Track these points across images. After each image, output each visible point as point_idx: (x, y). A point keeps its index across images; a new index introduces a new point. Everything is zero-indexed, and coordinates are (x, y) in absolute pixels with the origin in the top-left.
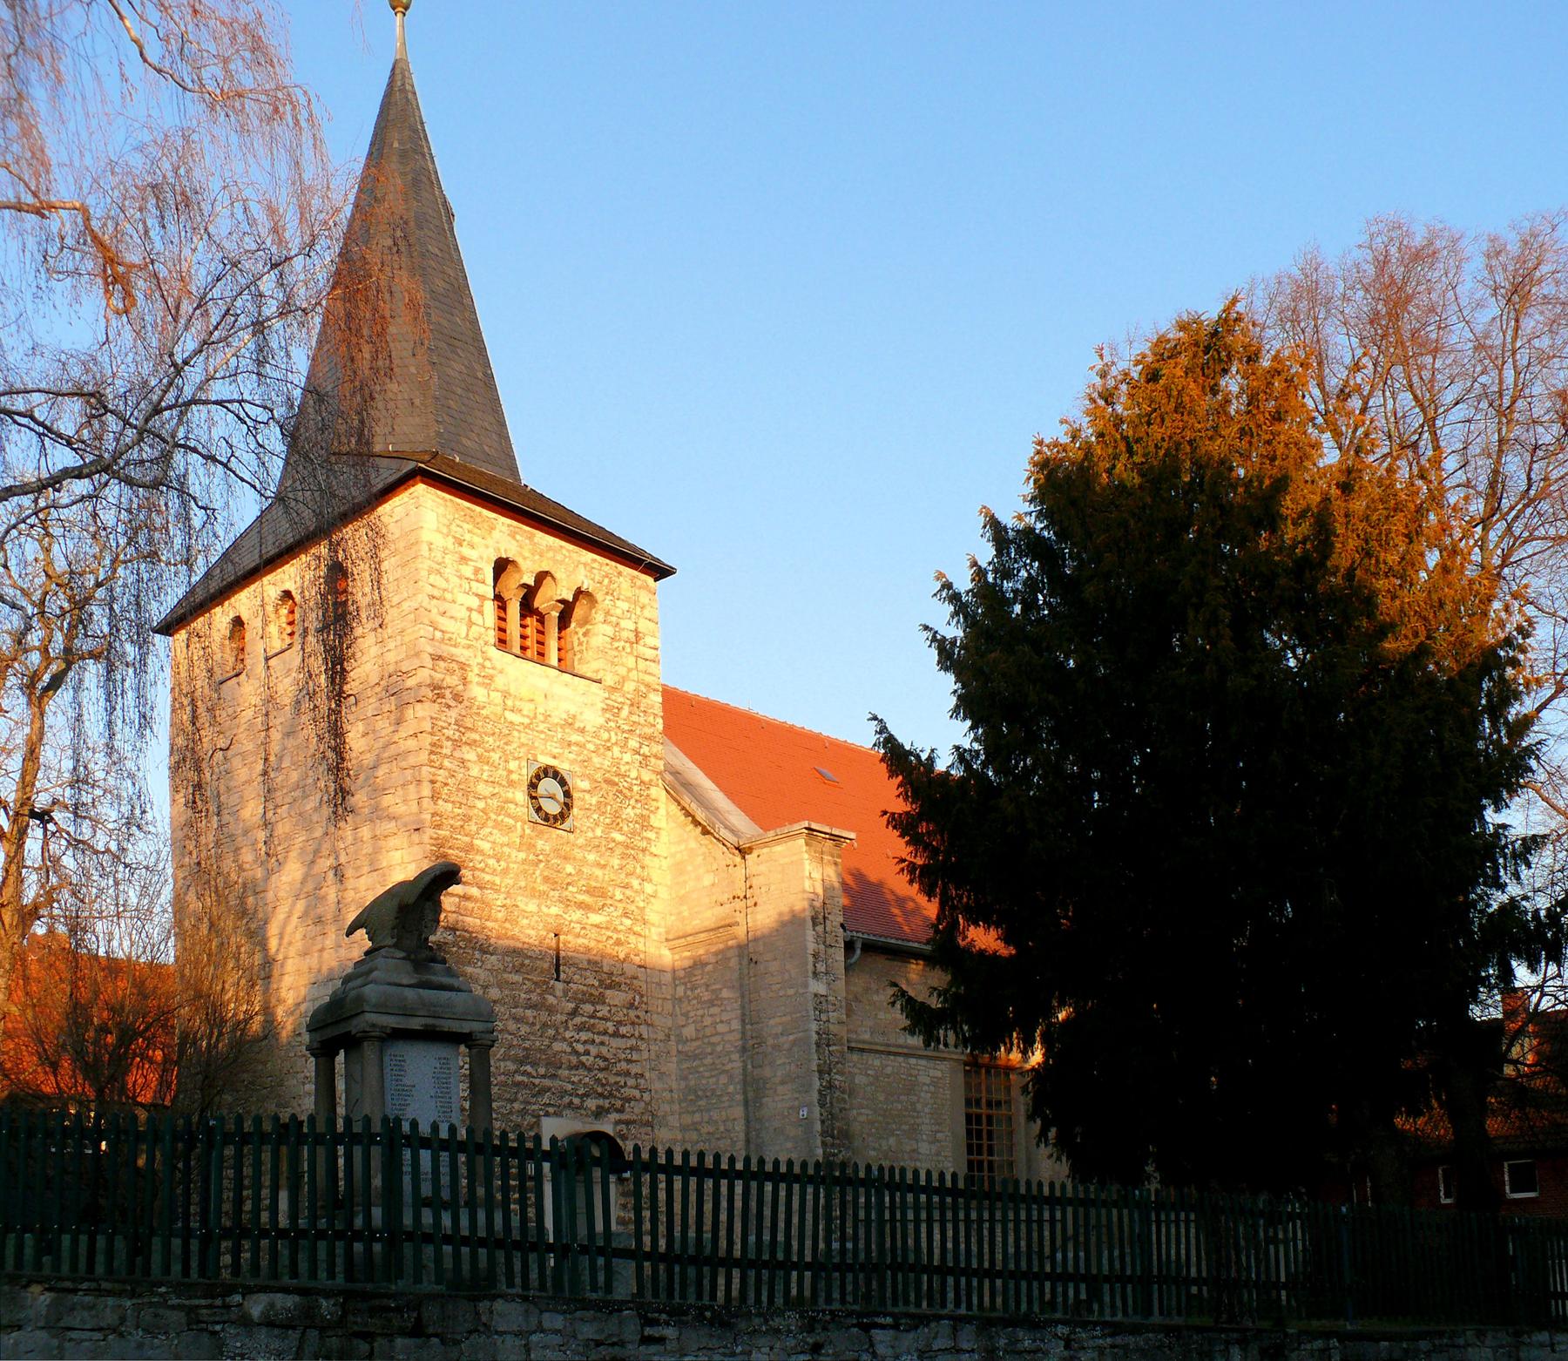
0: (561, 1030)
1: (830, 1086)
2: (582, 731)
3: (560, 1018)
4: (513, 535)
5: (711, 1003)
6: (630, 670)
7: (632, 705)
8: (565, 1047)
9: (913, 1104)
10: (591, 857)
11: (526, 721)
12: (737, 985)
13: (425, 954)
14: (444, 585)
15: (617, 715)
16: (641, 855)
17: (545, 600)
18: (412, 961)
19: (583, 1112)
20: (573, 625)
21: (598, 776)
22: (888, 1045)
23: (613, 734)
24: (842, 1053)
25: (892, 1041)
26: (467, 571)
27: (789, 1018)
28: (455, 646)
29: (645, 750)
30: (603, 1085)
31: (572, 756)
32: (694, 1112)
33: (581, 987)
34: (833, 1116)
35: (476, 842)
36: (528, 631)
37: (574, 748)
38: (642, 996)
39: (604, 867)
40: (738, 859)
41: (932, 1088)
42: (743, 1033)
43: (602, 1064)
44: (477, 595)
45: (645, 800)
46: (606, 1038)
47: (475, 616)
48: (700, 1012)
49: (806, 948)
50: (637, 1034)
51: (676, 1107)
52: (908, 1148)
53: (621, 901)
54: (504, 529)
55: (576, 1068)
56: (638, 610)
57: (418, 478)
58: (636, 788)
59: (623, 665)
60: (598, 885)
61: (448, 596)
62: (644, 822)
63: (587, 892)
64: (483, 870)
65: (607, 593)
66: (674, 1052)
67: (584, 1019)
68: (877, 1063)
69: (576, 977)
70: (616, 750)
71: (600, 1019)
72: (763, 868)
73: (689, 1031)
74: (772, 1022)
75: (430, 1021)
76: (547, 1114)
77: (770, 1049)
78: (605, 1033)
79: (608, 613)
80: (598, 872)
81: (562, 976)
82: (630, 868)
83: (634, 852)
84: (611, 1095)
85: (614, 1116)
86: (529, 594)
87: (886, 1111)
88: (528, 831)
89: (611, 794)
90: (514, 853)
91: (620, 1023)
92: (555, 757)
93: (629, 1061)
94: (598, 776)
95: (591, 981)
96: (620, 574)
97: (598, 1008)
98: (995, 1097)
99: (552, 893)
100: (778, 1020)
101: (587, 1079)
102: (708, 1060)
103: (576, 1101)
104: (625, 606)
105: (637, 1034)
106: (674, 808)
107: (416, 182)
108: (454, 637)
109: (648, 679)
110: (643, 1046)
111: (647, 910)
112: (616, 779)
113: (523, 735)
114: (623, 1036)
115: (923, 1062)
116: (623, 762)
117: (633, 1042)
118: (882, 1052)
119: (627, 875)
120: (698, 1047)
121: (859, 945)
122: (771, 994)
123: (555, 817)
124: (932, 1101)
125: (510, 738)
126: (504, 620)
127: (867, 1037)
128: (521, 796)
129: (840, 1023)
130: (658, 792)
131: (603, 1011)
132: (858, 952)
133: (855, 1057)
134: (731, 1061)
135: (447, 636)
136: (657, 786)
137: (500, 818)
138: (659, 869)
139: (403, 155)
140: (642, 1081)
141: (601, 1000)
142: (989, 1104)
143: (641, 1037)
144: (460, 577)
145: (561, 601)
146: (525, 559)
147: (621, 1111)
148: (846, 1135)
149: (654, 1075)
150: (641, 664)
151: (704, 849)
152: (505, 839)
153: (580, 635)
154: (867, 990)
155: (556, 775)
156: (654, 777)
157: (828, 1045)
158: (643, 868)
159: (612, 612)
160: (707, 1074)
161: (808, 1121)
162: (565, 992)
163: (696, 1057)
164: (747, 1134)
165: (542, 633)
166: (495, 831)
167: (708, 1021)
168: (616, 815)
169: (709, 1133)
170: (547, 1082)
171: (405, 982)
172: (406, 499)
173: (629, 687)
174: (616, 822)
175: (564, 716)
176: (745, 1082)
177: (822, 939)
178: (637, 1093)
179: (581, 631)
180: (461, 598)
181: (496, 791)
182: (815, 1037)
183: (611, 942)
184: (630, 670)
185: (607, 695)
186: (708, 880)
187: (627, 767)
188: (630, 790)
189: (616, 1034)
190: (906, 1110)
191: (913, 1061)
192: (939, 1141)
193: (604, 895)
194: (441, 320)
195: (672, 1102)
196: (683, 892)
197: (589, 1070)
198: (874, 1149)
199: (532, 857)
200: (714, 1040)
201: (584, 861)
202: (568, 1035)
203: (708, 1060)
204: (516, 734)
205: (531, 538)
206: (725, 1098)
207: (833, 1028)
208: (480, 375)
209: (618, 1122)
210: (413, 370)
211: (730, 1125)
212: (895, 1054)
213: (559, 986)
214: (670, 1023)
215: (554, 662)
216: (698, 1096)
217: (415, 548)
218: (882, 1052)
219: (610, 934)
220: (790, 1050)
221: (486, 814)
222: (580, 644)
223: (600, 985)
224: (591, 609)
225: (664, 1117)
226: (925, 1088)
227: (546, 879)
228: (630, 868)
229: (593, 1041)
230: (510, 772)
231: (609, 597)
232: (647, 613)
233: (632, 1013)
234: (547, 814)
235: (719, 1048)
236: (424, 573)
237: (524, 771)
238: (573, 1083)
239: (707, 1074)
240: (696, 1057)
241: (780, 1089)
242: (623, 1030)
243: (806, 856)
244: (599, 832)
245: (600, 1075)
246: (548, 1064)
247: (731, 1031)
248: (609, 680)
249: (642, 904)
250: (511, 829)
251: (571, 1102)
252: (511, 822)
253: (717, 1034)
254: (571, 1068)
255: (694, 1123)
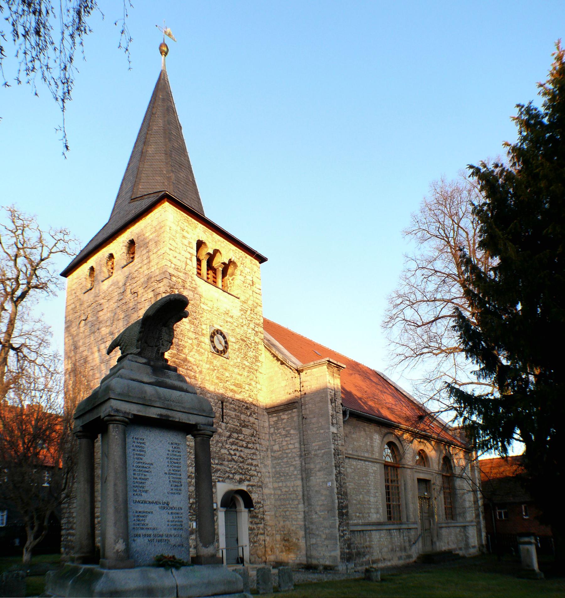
0: (224, 444)
1: (340, 473)
2: (232, 317)
3: (224, 439)
4: (204, 232)
5: (286, 436)
6: (250, 296)
7: (251, 310)
8: (226, 451)
9: (368, 481)
10: (236, 370)
11: (210, 309)
12: (297, 428)
13: (160, 363)
14: (176, 245)
15: (245, 313)
16: (255, 372)
17: (217, 262)
18: (152, 366)
19: (234, 480)
20: (228, 276)
21: (239, 337)
22: (358, 456)
23: (244, 320)
24: (343, 458)
25: (360, 454)
26: (186, 242)
27: (321, 443)
28: (180, 272)
29: (256, 329)
30: (242, 469)
31: (228, 327)
32: (279, 482)
33: (232, 426)
34: (341, 486)
35: (188, 358)
36: (209, 276)
37: (228, 324)
38: (257, 432)
39: (241, 375)
40: (297, 375)
41: (374, 475)
42: (300, 449)
43: (242, 460)
44: (189, 253)
45: (256, 350)
46: (243, 449)
47: (189, 262)
48: (281, 440)
49: (328, 412)
50: (255, 448)
51: (271, 480)
52: (366, 500)
53: (248, 390)
54: (201, 229)
55: (231, 461)
56: (253, 273)
57: (166, 199)
58: (253, 344)
59: (247, 293)
60: (239, 383)
61: (177, 250)
62: (256, 359)
63: (234, 385)
64: (191, 370)
65: (241, 264)
66: (270, 456)
67: (234, 440)
68: (355, 463)
69: (230, 421)
70: (245, 327)
71: (241, 440)
72: (308, 378)
73: (276, 447)
74: (313, 444)
75: (164, 412)
76: (219, 481)
77: (313, 456)
78: (242, 446)
79: (241, 271)
80: (239, 377)
81: (225, 420)
82: (251, 377)
83: (252, 370)
84: (245, 474)
85: (246, 483)
86: (211, 258)
87: (358, 483)
88: (210, 356)
89: (243, 345)
90: (204, 365)
91: (248, 443)
92: (221, 326)
93: (252, 459)
94: (239, 337)
95: (236, 423)
96: (246, 257)
97: (240, 435)
98: (393, 478)
99: (220, 384)
100: (316, 443)
101: (235, 466)
102: (285, 460)
103: (231, 476)
104: (248, 270)
105: (255, 448)
106: (268, 354)
107: (168, 110)
108: (180, 268)
109: (257, 301)
110: (258, 453)
111: (258, 395)
112: (245, 339)
113: (208, 315)
114: (250, 448)
115: (370, 464)
116: (248, 333)
117: (253, 451)
118: (356, 459)
119: (251, 380)
120: (280, 454)
121: (348, 413)
122: (313, 432)
123: (221, 351)
124: (374, 480)
125: (202, 315)
126: (200, 270)
127: (351, 452)
128: (207, 340)
129: (342, 445)
130: (261, 347)
131: (241, 437)
132: (348, 416)
133: (347, 460)
134: (295, 461)
135: (177, 267)
136: (261, 344)
137: (198, 349)
138: (262, 378)
139: (163, 100)
140: (257, 468)
141: (240, 432)
142: (392, 481)
143: (256, 449)
144: (183, 244)
145: (224, 263)
146: (209, 242)
147: (249, 481)
148: (346, 494)
149: (262, 465)
150: (255, 295)
151: (281, 371)
152: (201, 358)
153: (230, 280)
154: (350, 432)
155: (221, 334)
156: (260, 340)
157: (338, 455)
158: (256, 377)
159: (243, 271)
160: (284, 466)
161: (331, 488)
162: (226, 428)
163: (279, 458)
164: (303, 492)
165: (215, 278)
166: (196, 354)
167: (284, 443)
168: (246, 355)
169: (286, 491)
170: (219, 467)
171: (146, 379)
172: (160, 209)
173: (250, 303)
174: (245, 357)
175: (225, 310)
176: (302, 471)
177: (334, 409)
178: (255, 473)
179: (231, 278)
180: (183, 253)
181: (197, 337)
182: (333, 451)
183: (244, 407)
184: (250, 296)
185: (241, 304)
186: (283, 383)
187: (250, 335)
188: (251, 344)
189: (247, 447)
190: (365, 483)
191: (367, 463)
192: (377, 497)
193: (241, 387)
194: (176, 157)
195: (269, 477)
196: (272, 389)
197: (236, 462)
198: (355, 500)
199: (212, 367)
200: (287, 451)
201: (233, 371)
202: (227, 446)
203: (285, 460)
204: (205, 313)
205: (212, 235)
206: (293, 477)
207: (340, 448)
208: (191, 180)
209: (248, 486)
210: (165, 172)
211: (295, 489)
212: (361, 460)
213: (224, 425)
214: (268, 444)
215: (220, 286)
216: (280, 475)
217: (163, 228)
218: (356, 459)
219: (243, 404)
220: (322, 456)
221: (192, 346)
222: (230, 284)
223: (240, 426)
224: (235, 269)
225: (267, 484)
226: (372, 474)
227: (218, 378)
228: (251, 377)
229: (238, 450)
230: (203, 329)
231: (242, 265)
232: (256, 275)
233: (253, 439)
234: (218, 350)
235: (290, 455)
236: (167, 239)
237: (208, 330)
238: (230, 468)
239: (284, 466)
240: (279, 458)
241: (318, 474)
242: (250, 446)
243: (327, 373)
244: (239, 360)
245: (241, 465)
246: (219, 459)
247: (295, 448)
248: (242, 298)
249: (256, 393)
250: (202, 354)
251: (229, 476)
252: (203, 351)
253: (289, 449)
254: (228, 461)
255: (279, 487)
